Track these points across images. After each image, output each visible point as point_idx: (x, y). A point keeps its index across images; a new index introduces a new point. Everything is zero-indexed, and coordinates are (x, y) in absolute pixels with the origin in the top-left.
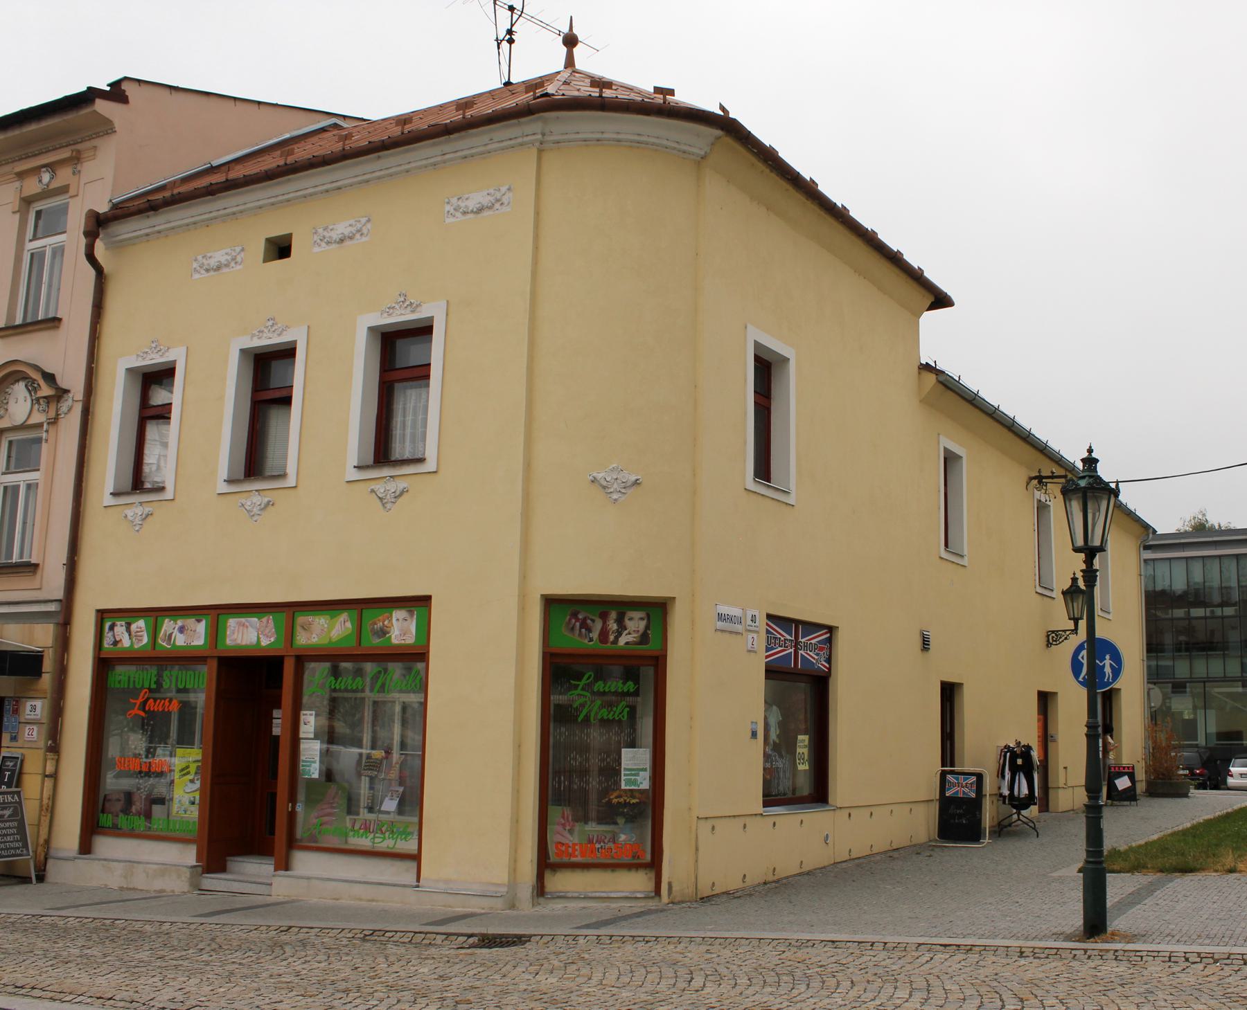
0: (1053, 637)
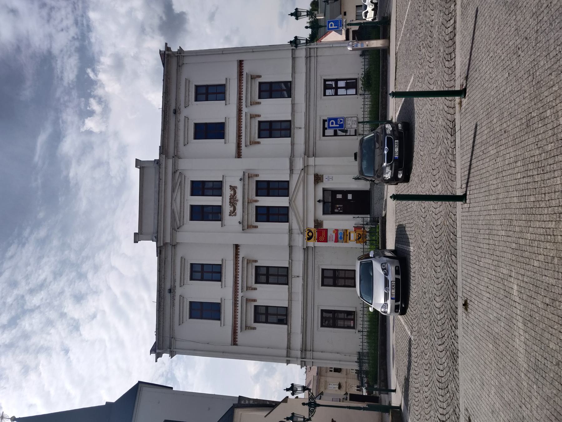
0: (312, 400)
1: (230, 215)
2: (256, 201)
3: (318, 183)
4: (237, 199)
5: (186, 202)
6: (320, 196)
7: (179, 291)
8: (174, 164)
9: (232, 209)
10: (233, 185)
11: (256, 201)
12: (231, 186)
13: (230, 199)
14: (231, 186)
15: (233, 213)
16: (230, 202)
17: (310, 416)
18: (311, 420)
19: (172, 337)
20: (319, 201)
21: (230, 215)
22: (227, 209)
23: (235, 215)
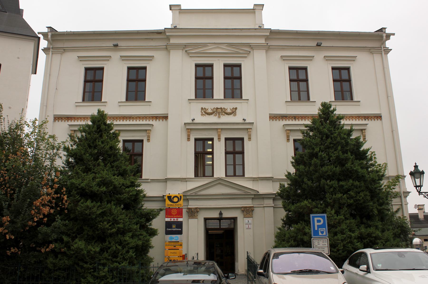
1: (202, 109)
2: (219, 139)
3: (243, 211)
4: (221, 116)
5: (217, 59)
6: (226, 214)
7: (116, 56)
8: (258, 47)
9: (210, 111)
10: (237, 111)
11: (219, 139)
12: (236, 109)
13: (221, 108)
14: (236, 109)
15: (205, 112)
16: (217, 108)
17: (424, 194)
18: (419, 194)
19: (65, 50)
20: (221, 214)
21: (202, 109)
22: (209, 105)
23: (202, 115)
